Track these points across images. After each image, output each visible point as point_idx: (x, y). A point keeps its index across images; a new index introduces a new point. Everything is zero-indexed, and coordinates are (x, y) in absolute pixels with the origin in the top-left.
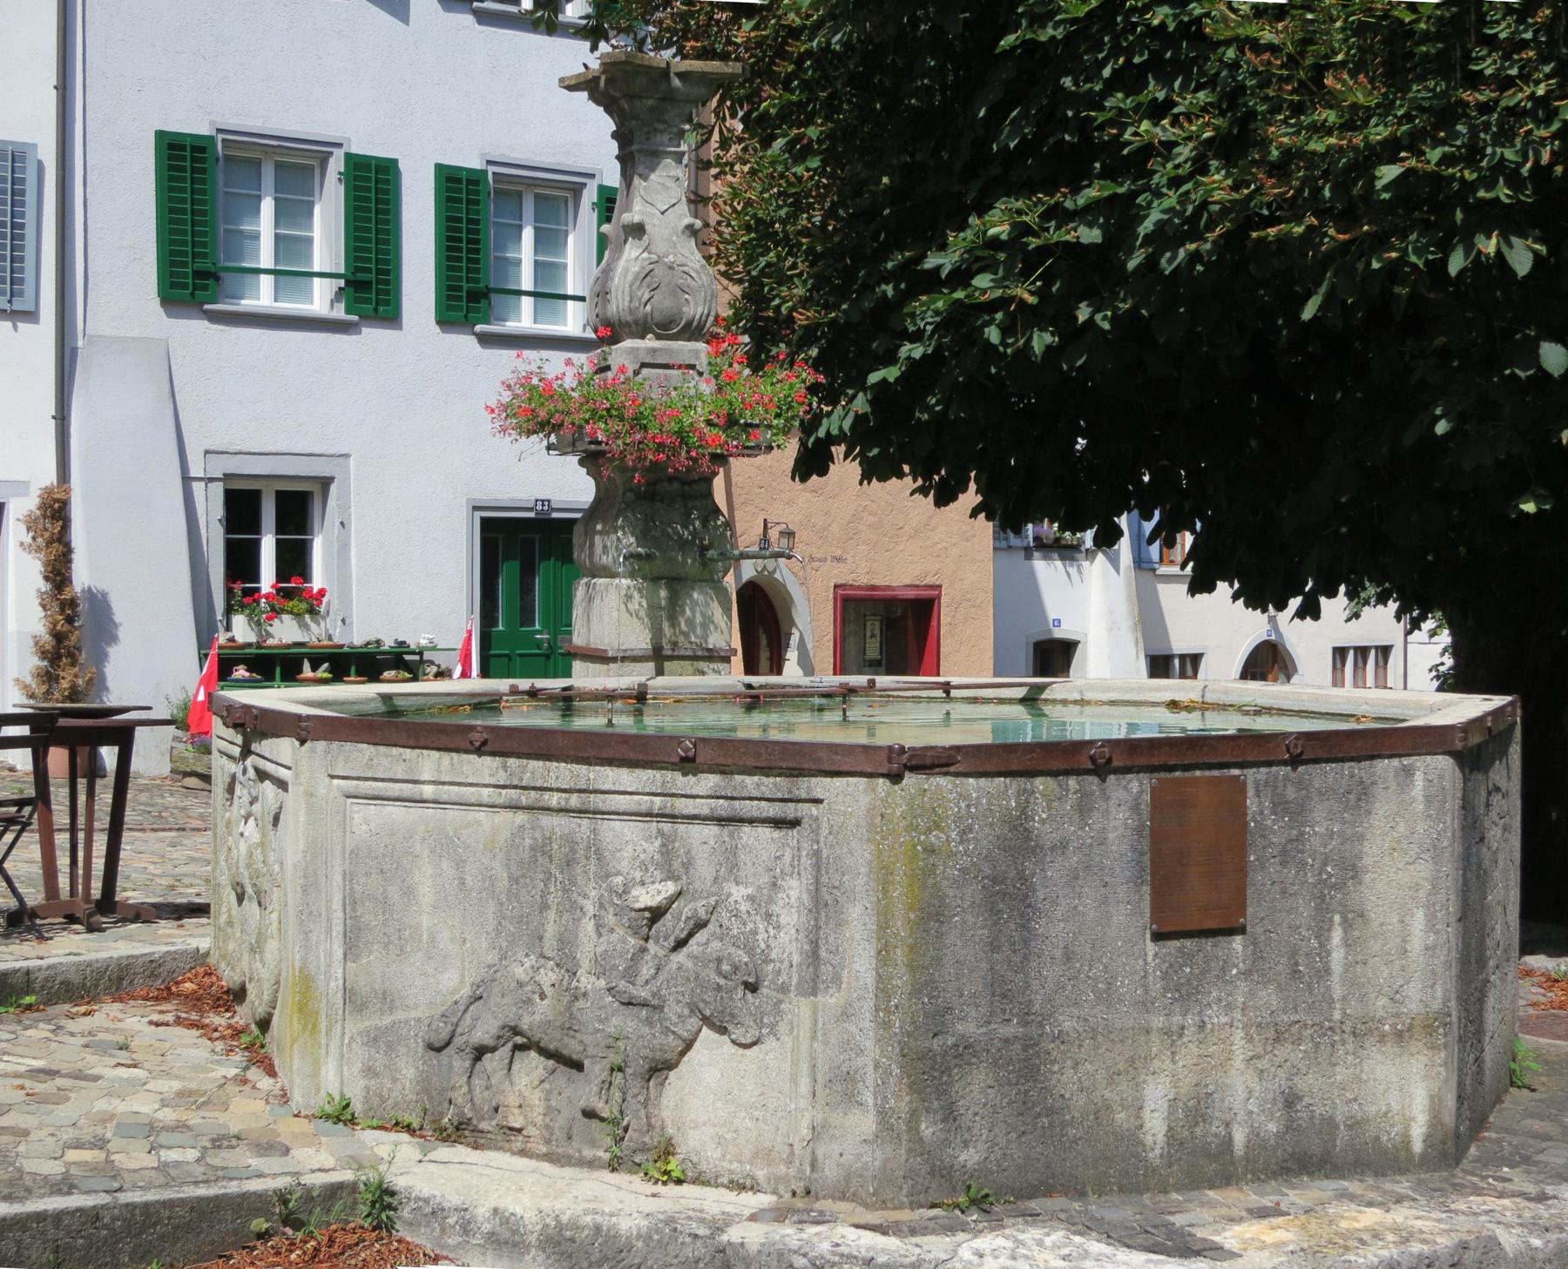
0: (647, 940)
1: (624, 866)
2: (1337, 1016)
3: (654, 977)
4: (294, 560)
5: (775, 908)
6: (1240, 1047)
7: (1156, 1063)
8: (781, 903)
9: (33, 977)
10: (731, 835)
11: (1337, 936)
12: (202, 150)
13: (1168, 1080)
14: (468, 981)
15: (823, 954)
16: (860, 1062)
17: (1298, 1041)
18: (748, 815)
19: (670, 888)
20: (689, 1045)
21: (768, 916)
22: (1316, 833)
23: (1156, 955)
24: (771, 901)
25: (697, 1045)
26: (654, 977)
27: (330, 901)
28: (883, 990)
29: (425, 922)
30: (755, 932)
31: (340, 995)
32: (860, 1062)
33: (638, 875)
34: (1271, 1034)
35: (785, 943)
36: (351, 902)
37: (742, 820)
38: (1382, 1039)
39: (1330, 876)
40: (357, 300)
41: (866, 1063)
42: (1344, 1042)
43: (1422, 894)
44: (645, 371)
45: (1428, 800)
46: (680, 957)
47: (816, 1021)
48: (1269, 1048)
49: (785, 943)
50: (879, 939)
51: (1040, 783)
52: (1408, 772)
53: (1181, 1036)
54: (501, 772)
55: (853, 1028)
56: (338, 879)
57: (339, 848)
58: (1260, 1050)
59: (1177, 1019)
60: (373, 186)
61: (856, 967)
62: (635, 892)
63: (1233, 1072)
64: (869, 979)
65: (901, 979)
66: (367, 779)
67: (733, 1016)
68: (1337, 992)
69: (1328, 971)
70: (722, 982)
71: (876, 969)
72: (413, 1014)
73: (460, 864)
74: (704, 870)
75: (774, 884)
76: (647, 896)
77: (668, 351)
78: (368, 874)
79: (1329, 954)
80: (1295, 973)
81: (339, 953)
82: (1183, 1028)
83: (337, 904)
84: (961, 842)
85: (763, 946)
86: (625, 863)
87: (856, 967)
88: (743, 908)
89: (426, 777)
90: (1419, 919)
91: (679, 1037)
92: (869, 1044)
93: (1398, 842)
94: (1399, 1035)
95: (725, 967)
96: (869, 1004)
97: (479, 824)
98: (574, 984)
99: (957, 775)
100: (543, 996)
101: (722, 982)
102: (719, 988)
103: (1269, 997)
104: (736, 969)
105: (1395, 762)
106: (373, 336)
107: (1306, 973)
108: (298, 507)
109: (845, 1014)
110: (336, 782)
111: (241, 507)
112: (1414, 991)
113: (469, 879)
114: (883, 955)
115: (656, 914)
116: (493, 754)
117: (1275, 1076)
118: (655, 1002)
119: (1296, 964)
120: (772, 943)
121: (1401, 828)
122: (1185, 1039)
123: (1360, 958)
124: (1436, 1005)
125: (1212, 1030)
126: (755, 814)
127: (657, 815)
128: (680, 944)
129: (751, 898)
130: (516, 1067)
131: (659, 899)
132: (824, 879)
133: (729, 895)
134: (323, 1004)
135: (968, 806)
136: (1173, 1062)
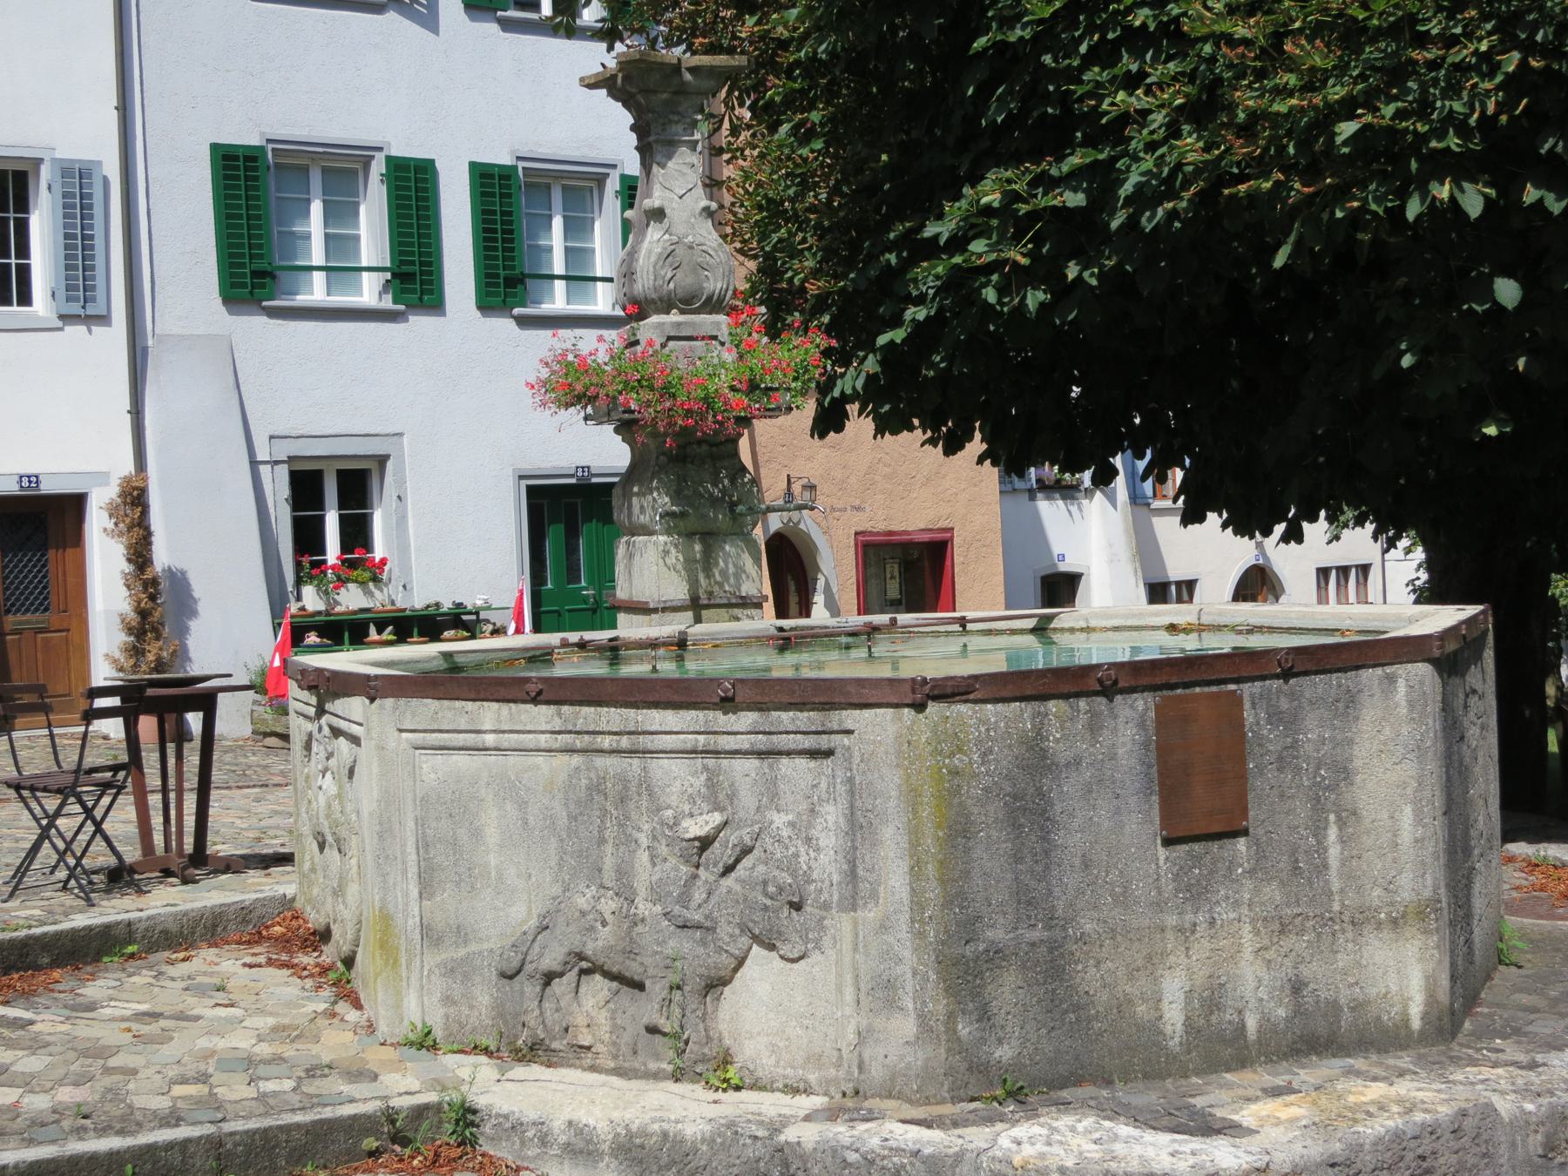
0: (697, 867)
1: (673, 800)
2: (1336, 907)
4: (356, 533)
7: (1172, 959)
8: (819, 828)
9: (134, 928)
10: (771, 767)
14: (535, 912)
15: (861, 872)
16: (899, 970)
20: (741, 962)
21: (808, 840)
24: (810, 826)
25: (748, 962)
27: (403, 846)
28: (917, 904)
29: (493, 860)
30: (796, 855)
31: (418, 931)
32: (899, 970)
34: (1277, 927)
36: (424, 845)
37: (780, 753)
39: (1324, 778)
40: (403, 291)
41: (904, 970)
42: (1343, 931)
43: (1409, 791)
44: (671, 344)
45: (1411, 705)
46: (729, 881)
47: (857, 935)
49: (824, 863)
50: (911, 857)
51: (1053, 706)
52: (1391, 679)
53: (1193, 932)
55: (891, 940)
56: (411, 824)
57: (410, 795)
58: (1266, 942)
59: (1189, 917)
64: (904, 893)
65: (933, 892)
68: (1336, 885)
70: (769, 902)
72: (486, 946)
73: (522, 805)
74: (748, 799)
75: (812, 811)
76: (695, 828)
79: (1326, 850)
81: (415, 893)
82: (1195, 925)
84: (983, 763)
87: (892, 883)
88: (785, 833)
90: (1407, 815)
92: (907, 953)
93: (1385, 744)
94: (1394, 922)
95: (771, 889)
96: (905, 917)
97: (538, 768)
98: (633, 911)
99: (976, 702)
100: (604, 923)
101: (769, 902)
105: (1379, 671)
107: (1304, 869)
110: (404, 735)
112: (1406, 880)
113: (531, 818)
114: (916, 871)
115: (705, 843)
116: (548, 702)
118: (708, 924)
121: (1387, 731)
123: (1355, 852)
124: (1427, 893)
126: (792, 746)
128: (729, 869)
129: (792, 824)
130: (582, 989)
131: (707, 829)
132: (858, 803)
133: (772, 822)
136: (1188, 957)
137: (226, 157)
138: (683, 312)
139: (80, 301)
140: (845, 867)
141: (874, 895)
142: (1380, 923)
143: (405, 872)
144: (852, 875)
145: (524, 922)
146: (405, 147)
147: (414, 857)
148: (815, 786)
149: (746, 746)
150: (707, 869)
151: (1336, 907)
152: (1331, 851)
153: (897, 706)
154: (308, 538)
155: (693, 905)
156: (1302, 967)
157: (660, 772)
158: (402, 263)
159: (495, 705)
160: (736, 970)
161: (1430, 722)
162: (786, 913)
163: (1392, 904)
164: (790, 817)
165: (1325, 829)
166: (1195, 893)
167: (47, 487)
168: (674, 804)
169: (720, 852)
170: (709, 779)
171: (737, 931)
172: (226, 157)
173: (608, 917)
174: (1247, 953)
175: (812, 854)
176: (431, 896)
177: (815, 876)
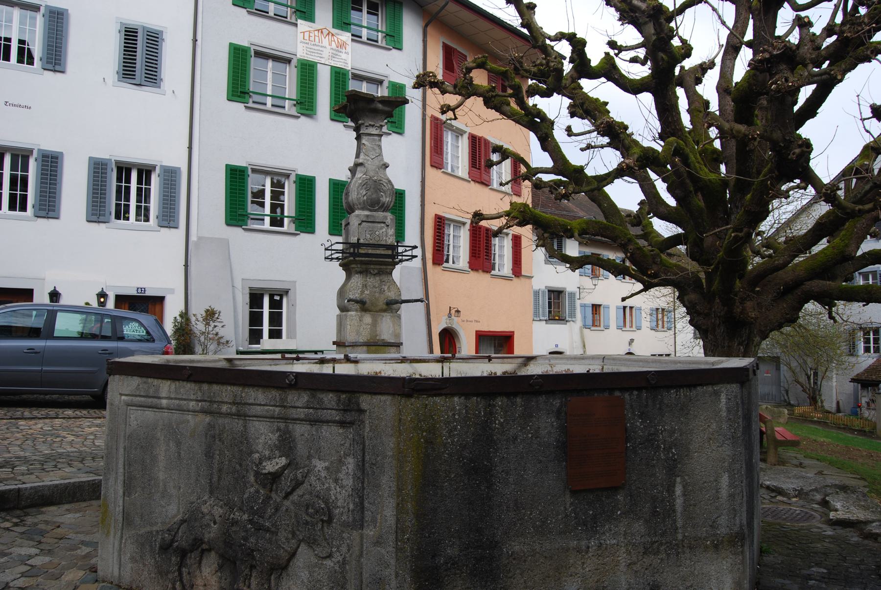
0: (271, 491)
1: (260, 448)
2: (680, 537)
3: (274, 514)
4: (276, 319)
5: (341, 476)
6: (622, 557)
7: (572, 569)
8: (344, 472)
9: (21, 493)
10: (317, 431)
11: (678, 490)
12: (243, 171)
13: (580, 580)
14: (181, 510)
15: (366, 504)
16: (387, 572)
17: (657, 553)
18: (325, 419)
19: (283, 461)
20: (293, 555)
21: (336, 481)
22: (665, 430)
23: (571, 504)
24: (339, 471)
25: (297, 556)
26: (274, 514)
27: (117, 463)
28: (400, 529)
29: (161, 476)
30: (329, 489)
31: (121, 515)
32: (387, 572)
33: (267, 453)
34: (642, 550)
35: (341, 495)
36: (128, 464)
37: (323, 422)
38: (706, 548)
39: (674, 454)
40: (300, 226)
41: (390, 572)
42: (684, 553)
43: (726, 464)
44: (364, 224)
45: (729, 411)
46: (287, 503)
47: (362, 545)
48: (640, 558)
49: (341, 495)
50: (398, 497)
51: (499, 401)
52: (717, 394)
53: (587, 552)
54: (199, 393)
55: (383, 551)
56: (121, 450)
57: (123, 433)
58: (634, 559)
59: (584, 543)
60: (306, 185)
61: (385, 513)
62: (264, 464)
63: (619, 573)
64: (391, 521)
65: (410, 521)
66: (136, 396)
67: (315, 540)
68: (680, 523)
69: (674, 511)
70: (309, 519)
71: (397, 515)
72: (155, 528)
73: (178, 444)
74: (301, 449)
75: (340, 461)
76: (270, 467)
77: (373, 216)
78: (136, 448)
79: (674, 500)
80: (654, 513)
81: (121, 492)
82: (588, 547)
83: (121, 465)
84: (450, 437)
85: (333, 498)
86: (260, 446)
87: (385, 513)
88: (323, 475)
89: (164, 395)
90: (725, 480)
91: (286, 551)
92: (393, 562)
93: (712, 434)
94: (716, 547)
95: (311, 511)
96: (392, 537)
97: (188, 421)
98: (232, 516)
99: (446, 395)
100: (215, 523)
101: (309, 519)
102: (307, 523)
103: (639, 527)
104: (317, 512)
105: (710, 389)
106: (304, 237)
107: (660, 514)
108: (277, 298)
109: (378, 542)
110: (123, 397)
111: (255, 299)
112: (723, 520)
113: (183, 453)
114: (400, 508)
115: (275, 477)
116: (195, 382)
117: (644, 574)
118: (273, 529)
119: (656, 507)
120: (339, 497)
121: (714, 426)
122: (590, 555)
123: (692, 502)
124: (736, 529)
125: (606, 548)
126: (329, 418)
127: (277, 418)
128: (287, 495)
129: (327, 468)
130: (204, 561)
131: (277, 468)
132: (367, 458)
133: (315, 466)
134: (112, 521)
135: (454, 415)
136: (584, 569)
137: (231, 170)
138: (371, 211)
139: (168, 219)
140: (357, 500)
141: (374, 521)
142: (706, 547)
143: (116, 479)
144: (361, 507)
145: (176, 516)
146: (305, 171)
147: (121, 470)
148: (342, 445)
149: (303, 416)
150: (276, 493)
151: (680, 537)
152: (678, 501)
153: (394, 394)
154: (255, 319)
155: (267, 516)
156: (657, 575)
157: (253, 429)
158: (300, 215)
159: (169, 382)
160: (289, 560)
161: (740, 420)
162: (320, 525)
163: (715, 535)
164: (327, 464)
165: (674, 486)
166: (591, 526)
167: (148, 293)
168: (260, 450)
169: (285, 484)
170: (280, 436)
171: (290, 536)
172: (231, 170)
173: (217, 518)
174: (622, 567)
175: (338, 490)
176: (129, 495)
177: (339, 504)
